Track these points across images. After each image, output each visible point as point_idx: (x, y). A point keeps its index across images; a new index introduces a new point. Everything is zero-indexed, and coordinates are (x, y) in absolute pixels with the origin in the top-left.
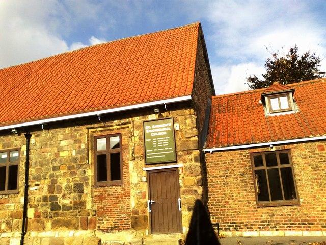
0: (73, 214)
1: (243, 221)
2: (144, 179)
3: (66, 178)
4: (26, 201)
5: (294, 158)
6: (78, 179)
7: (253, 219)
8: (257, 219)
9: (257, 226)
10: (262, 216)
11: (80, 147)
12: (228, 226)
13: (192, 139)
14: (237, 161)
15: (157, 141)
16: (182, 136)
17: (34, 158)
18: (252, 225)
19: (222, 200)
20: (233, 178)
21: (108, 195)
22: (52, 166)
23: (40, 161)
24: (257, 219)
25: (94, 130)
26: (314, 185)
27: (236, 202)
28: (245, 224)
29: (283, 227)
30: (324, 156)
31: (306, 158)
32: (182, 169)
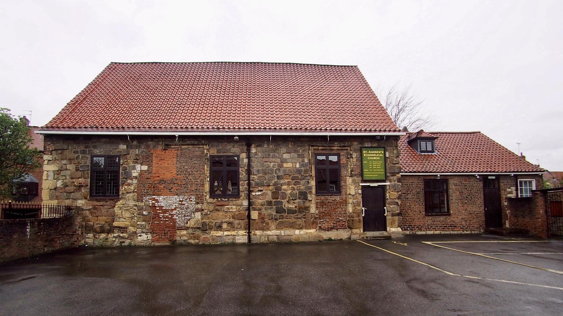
0: (297, 217)
1: (416, 224)
2: (360, 191)
4: (250, 204)
5: (450, 185)
6: (302, 188)
10: (428, 222)
12: (407, 227)
14: (415, 183)
15: (372, 164)
16: (390, 162)
18: (421, 227)
19: (403, 209)
20: (412, 195)
21: (329, 202)
22: (276, 175)
23: (262, 170)
25: (317, 148)
26: (459, 203)
27: (412, 212)
28: (417, 226)
30: (466, 186)
31: (457, 186)
32: (389, 186)
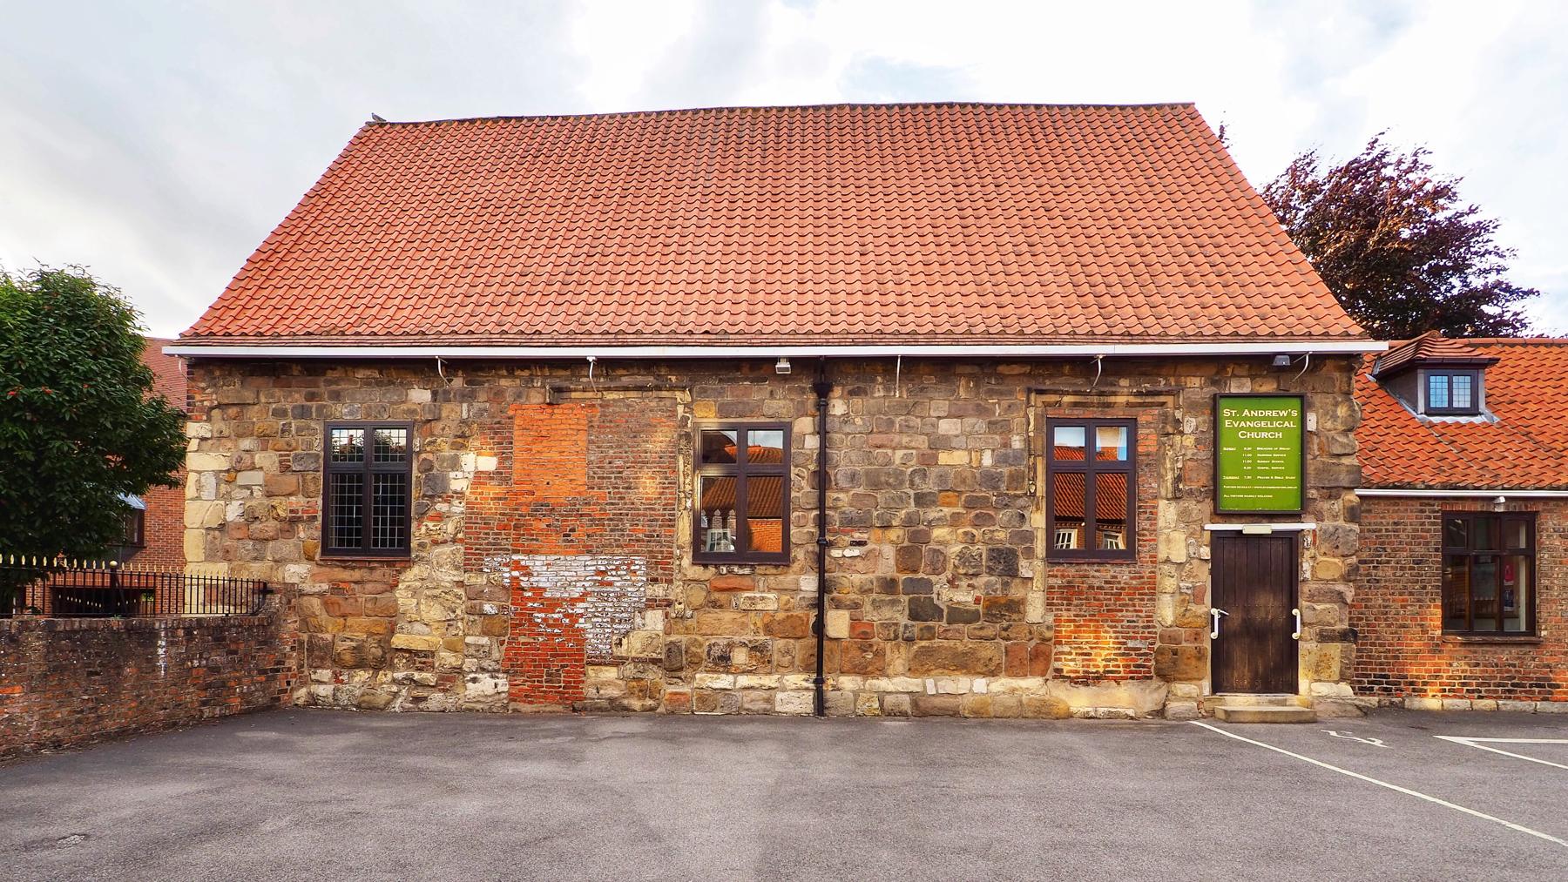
0: (982, 633)
2: (1206, 552)
3: (960, 531)
4: (824, 587)
7: (1429, 671)
8: (1439, 671)
9: (1438, 687)
10: (1451, 665)
11: (1006, 445)
12: (1369, 683)
13: (1346, 461)
14: (1409, 527)
16: (1320, 449)
17: (845, 459)
18: (1425, 684)
21: (1091, 587)
22: (912, 493)
23: (867, 473)
24: (1439, 671)
25: (1053, 398)
29: (1496, 691)
32: (1315, 536)
